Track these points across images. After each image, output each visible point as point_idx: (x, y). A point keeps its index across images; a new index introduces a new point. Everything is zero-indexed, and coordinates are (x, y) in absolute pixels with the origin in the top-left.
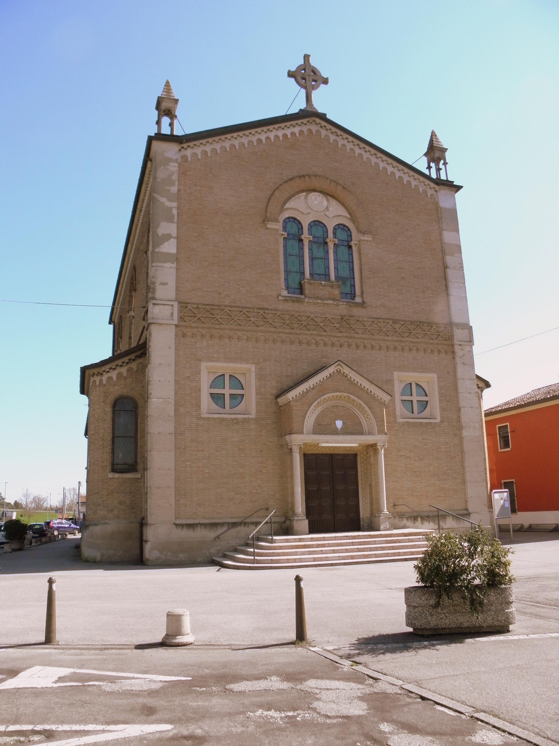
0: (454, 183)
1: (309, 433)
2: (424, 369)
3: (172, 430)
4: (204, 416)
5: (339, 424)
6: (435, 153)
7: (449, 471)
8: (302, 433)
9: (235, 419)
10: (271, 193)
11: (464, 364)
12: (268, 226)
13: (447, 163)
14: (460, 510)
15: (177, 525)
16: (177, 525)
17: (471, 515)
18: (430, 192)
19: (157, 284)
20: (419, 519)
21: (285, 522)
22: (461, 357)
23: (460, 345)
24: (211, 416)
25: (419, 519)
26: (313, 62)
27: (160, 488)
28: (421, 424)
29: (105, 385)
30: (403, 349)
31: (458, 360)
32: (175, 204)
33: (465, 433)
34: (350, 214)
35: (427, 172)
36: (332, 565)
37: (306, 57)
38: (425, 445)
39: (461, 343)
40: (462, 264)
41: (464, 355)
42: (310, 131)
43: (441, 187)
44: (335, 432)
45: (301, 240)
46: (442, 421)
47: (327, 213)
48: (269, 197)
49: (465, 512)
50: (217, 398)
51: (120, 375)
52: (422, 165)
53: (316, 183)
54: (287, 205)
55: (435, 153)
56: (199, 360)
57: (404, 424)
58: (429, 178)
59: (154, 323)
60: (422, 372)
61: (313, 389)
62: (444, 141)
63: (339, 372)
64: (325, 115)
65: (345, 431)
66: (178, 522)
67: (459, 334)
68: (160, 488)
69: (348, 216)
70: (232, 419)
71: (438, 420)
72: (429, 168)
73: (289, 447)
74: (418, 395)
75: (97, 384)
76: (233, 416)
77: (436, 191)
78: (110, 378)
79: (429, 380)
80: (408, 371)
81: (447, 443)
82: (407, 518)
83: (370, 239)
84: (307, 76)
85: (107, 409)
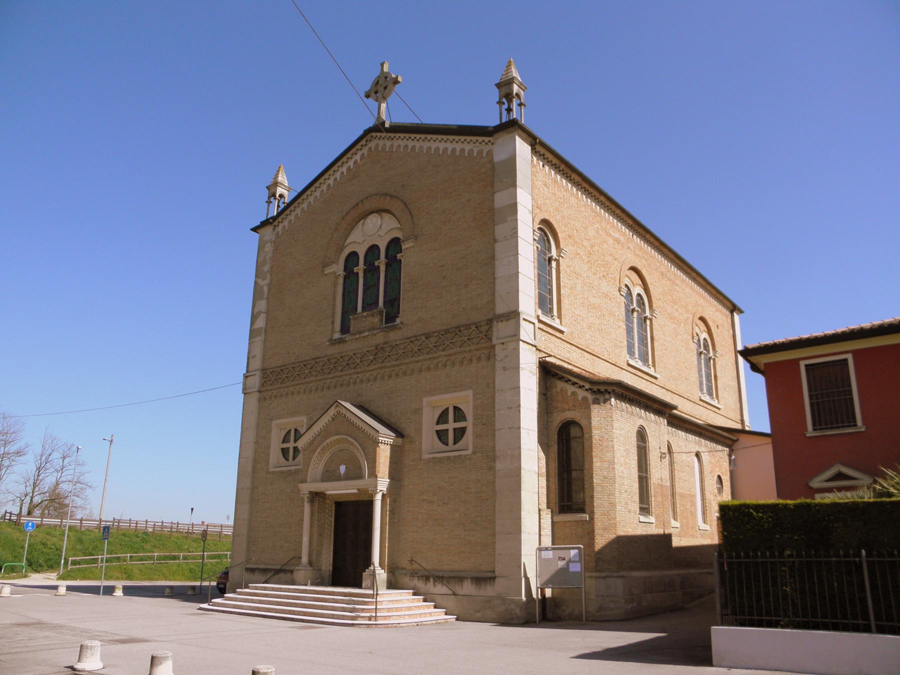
1: (315, 481)
2: (458, 387)
5: (343, 469)
7: (478, 518)
8: (306, 482)
9: (290, 471)
11: (505, 369)
13: (498, 103)
14: (485, 572)
15: (247, 569)
16: (247, 569)
17: (497, 580)
20: (432, 580)
22: (501, 360)
23: (503, 344)
24: (278, 469)
25: (432, 580)
28: (449, 458)
30: (397, 375)
31: (499, 365)
33: (499, 466)
36: (323, 623)
38: (452, 485)
39: (502, 341)
41: (506, 356)
43: (496, 135)
44: (338, 478)
46: (474, 453)
49: (490, 575)
50: (442, 435)
53: (368, 206)
54: (348, 241)
56: (272, 420)
57: (429, 460)
60: (454, 392)
61: (318, 435)
63: (339, 413)
65: (348, 477)
66: (248, 566)
67: (255, 381)
70: (288, 471)
71: (469, 452)
74: (446, 422)
76: (288, 468)
79: (465, 399)
80: (440, 394)
81: (479, 481)
82: (419, 577)
83: (412, 244)
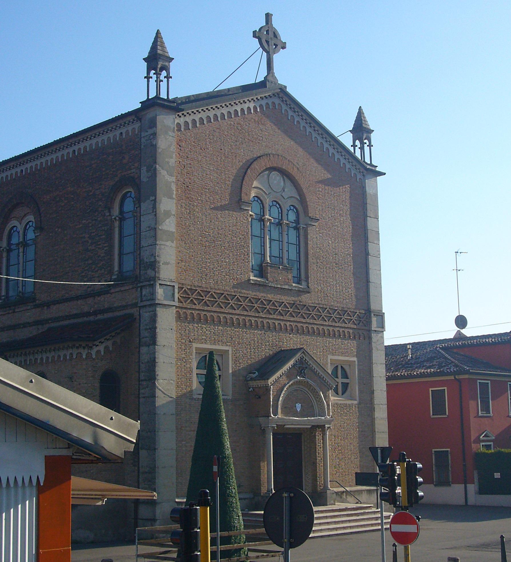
0: (377, 169)
3: (174, 411)
4: (195, 397)
6: (361, 130)
10: (244, 171)
12: (242, 207)
18: (359, 176)
19: (161, 264)
21: (254, 498)
26: (276, 23)
27: (165, 467)
29: (94, 359)
32: (173, 179)
34: (300, 195)
35: (352, 149)
37: (268, 17)
40: (379, 251)
42: (274, 103)
45: (263, 220)
47: (283, 194)
48: (242, 175)
51: (106, 348)
52: (347, 140)
55: (361, 130)
58: (352, 156)
59: (159, 304)
62: (371, 122)
64: (286, 87)
68: (165, 467)
69: (298, 197)
72: (354, 146)
73: (262, 428)
75: (84, 357)
77: (363, 175)
78: (98, 352)
84: (269, 39)
85: (96, 385)
